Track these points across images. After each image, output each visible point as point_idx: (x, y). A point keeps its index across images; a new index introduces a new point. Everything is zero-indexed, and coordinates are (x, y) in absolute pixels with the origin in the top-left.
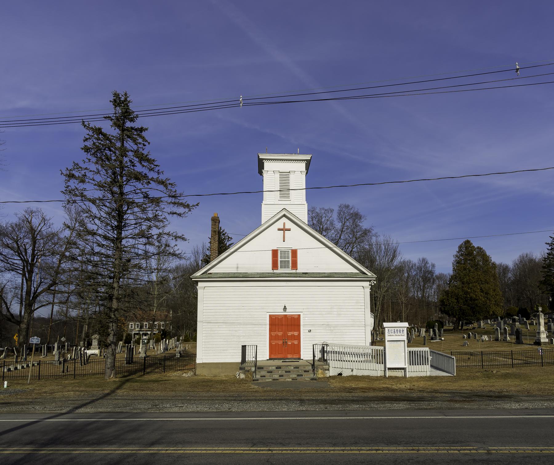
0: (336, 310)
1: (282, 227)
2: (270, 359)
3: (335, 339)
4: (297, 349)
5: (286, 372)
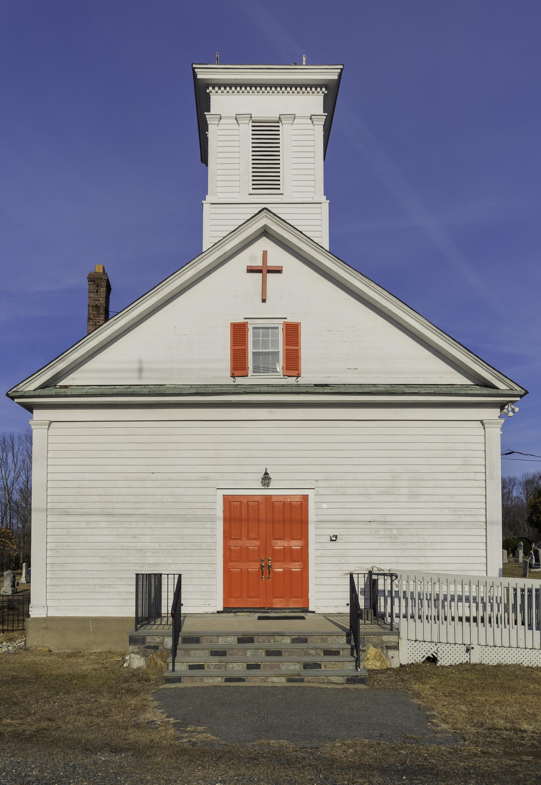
0: (406, 483)
1: (259, 263)
2: (227, 610)
3: (402, 560)
4: (299, 584)
5: (269, 653)
